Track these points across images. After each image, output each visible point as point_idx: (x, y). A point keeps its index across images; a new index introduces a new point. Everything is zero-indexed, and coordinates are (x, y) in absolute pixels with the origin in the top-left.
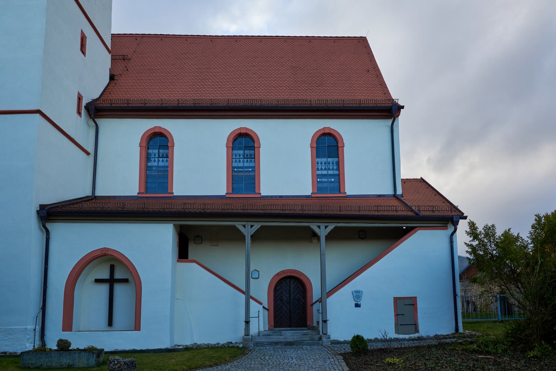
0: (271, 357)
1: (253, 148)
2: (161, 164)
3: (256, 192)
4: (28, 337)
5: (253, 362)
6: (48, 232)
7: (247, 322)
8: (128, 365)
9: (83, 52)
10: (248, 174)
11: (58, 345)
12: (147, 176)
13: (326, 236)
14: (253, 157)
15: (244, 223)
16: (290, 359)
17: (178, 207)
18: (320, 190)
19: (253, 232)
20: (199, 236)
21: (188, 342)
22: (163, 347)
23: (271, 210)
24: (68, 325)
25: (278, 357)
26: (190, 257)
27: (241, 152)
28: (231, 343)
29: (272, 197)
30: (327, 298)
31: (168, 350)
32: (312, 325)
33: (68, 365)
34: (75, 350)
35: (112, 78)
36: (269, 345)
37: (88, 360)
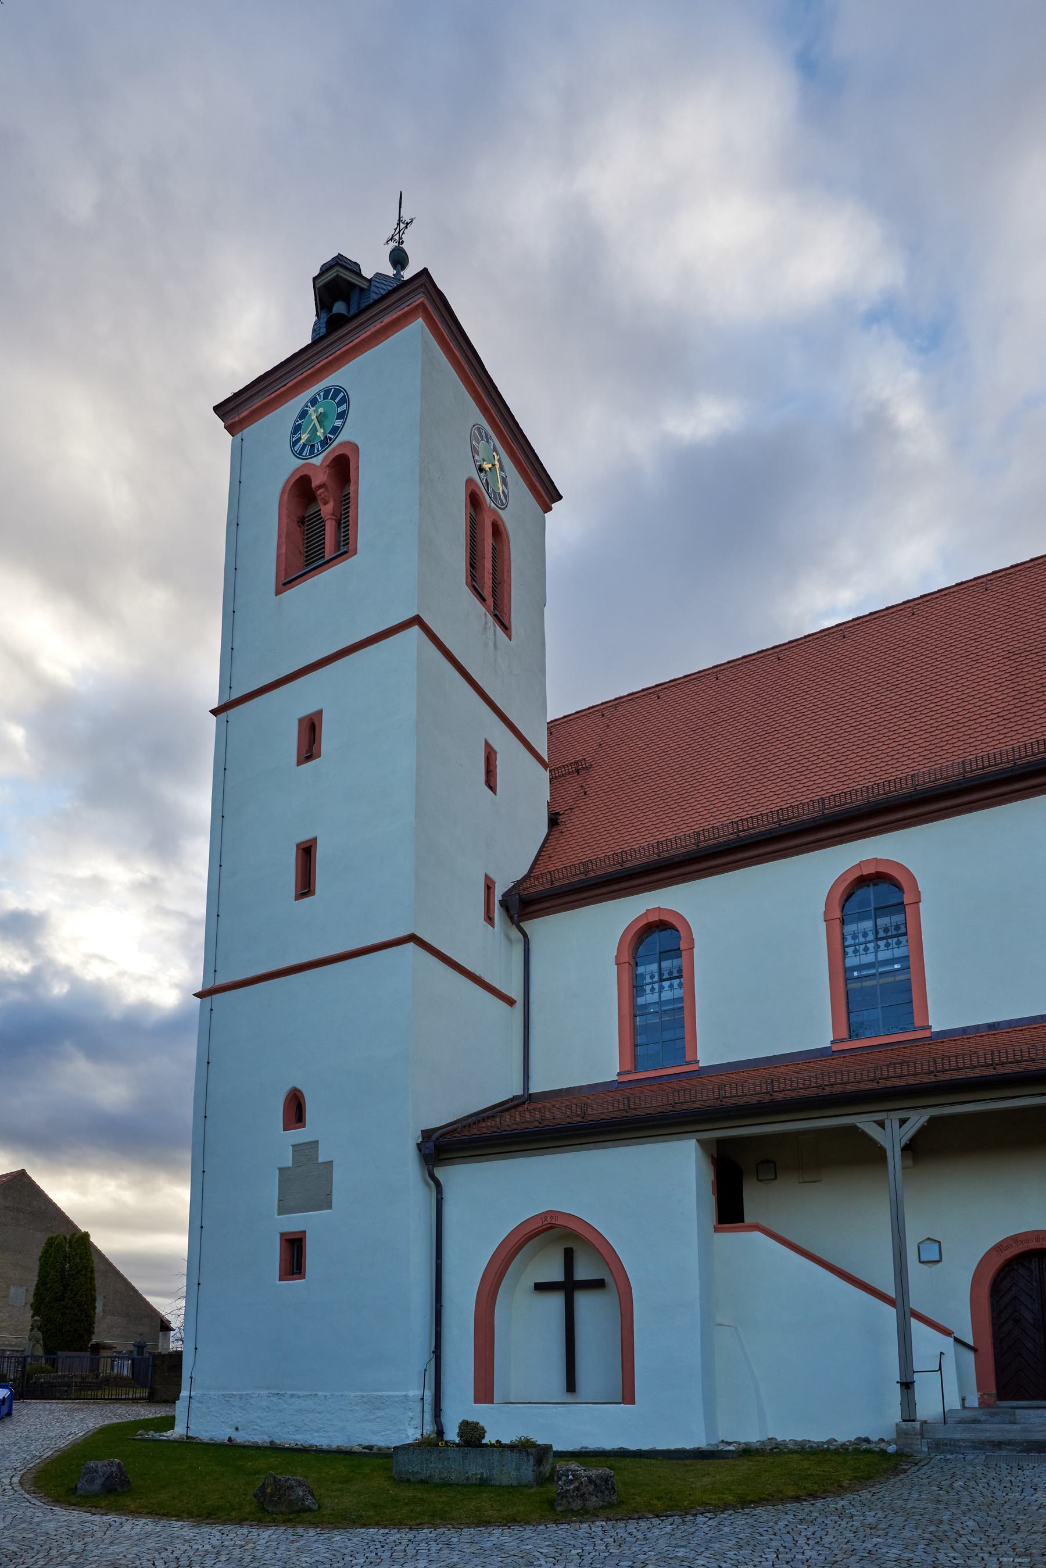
0: (972, 1484)
1: (900, 907)
2: (667, 995)
3: (918, 1022)
4: (411, 1414)
5: (915, 1495)
6: (438, 1185)
7: (907, 1386)
8: (596, 1485)
9: (491, 783)
10: (891, 979)
11: (460, 1435)
12: (635, 1030)
13: (905, 1149)
14: (902, 930)
16: (1029, 1491)
17: (705, 1097)
18: (853, 1033)
20: (767, 1162)
21: (752, 1435)
22: (689, 1446)
23: (958, 1069)
25: (993, 1483)
26: (748, 1219)
27: (868, 925)
28: (867, 1440)
29: (964, 1030)
31: (699, 1454)
33: (481, 1479)
34: (492, 1445)
35: (554, 821)
36: (975, 1448)
37: (518, 1469)
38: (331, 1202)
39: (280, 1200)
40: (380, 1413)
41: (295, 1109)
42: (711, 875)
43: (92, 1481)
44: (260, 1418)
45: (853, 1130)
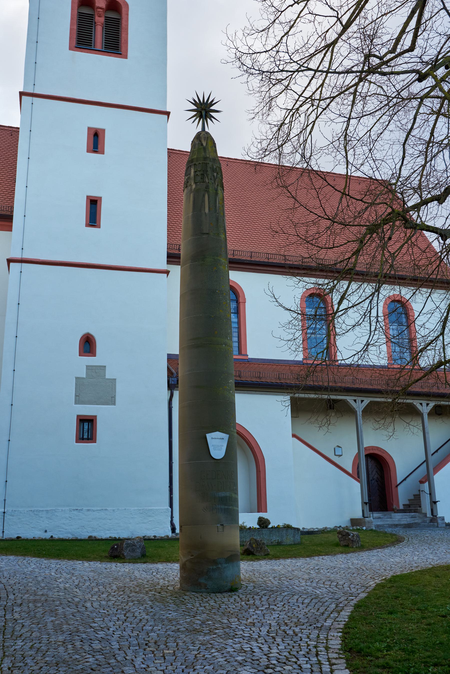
15: (355, 398)
19: (363, 408)
24: (261, 504)
30: (435, 473)
32: (398, 509)
36: (390, 527)
37: (294, 537)
39: (76, 396)
41: (88, 345)
42: (253, 272)
43: (133, 551)
44: (64, 524)
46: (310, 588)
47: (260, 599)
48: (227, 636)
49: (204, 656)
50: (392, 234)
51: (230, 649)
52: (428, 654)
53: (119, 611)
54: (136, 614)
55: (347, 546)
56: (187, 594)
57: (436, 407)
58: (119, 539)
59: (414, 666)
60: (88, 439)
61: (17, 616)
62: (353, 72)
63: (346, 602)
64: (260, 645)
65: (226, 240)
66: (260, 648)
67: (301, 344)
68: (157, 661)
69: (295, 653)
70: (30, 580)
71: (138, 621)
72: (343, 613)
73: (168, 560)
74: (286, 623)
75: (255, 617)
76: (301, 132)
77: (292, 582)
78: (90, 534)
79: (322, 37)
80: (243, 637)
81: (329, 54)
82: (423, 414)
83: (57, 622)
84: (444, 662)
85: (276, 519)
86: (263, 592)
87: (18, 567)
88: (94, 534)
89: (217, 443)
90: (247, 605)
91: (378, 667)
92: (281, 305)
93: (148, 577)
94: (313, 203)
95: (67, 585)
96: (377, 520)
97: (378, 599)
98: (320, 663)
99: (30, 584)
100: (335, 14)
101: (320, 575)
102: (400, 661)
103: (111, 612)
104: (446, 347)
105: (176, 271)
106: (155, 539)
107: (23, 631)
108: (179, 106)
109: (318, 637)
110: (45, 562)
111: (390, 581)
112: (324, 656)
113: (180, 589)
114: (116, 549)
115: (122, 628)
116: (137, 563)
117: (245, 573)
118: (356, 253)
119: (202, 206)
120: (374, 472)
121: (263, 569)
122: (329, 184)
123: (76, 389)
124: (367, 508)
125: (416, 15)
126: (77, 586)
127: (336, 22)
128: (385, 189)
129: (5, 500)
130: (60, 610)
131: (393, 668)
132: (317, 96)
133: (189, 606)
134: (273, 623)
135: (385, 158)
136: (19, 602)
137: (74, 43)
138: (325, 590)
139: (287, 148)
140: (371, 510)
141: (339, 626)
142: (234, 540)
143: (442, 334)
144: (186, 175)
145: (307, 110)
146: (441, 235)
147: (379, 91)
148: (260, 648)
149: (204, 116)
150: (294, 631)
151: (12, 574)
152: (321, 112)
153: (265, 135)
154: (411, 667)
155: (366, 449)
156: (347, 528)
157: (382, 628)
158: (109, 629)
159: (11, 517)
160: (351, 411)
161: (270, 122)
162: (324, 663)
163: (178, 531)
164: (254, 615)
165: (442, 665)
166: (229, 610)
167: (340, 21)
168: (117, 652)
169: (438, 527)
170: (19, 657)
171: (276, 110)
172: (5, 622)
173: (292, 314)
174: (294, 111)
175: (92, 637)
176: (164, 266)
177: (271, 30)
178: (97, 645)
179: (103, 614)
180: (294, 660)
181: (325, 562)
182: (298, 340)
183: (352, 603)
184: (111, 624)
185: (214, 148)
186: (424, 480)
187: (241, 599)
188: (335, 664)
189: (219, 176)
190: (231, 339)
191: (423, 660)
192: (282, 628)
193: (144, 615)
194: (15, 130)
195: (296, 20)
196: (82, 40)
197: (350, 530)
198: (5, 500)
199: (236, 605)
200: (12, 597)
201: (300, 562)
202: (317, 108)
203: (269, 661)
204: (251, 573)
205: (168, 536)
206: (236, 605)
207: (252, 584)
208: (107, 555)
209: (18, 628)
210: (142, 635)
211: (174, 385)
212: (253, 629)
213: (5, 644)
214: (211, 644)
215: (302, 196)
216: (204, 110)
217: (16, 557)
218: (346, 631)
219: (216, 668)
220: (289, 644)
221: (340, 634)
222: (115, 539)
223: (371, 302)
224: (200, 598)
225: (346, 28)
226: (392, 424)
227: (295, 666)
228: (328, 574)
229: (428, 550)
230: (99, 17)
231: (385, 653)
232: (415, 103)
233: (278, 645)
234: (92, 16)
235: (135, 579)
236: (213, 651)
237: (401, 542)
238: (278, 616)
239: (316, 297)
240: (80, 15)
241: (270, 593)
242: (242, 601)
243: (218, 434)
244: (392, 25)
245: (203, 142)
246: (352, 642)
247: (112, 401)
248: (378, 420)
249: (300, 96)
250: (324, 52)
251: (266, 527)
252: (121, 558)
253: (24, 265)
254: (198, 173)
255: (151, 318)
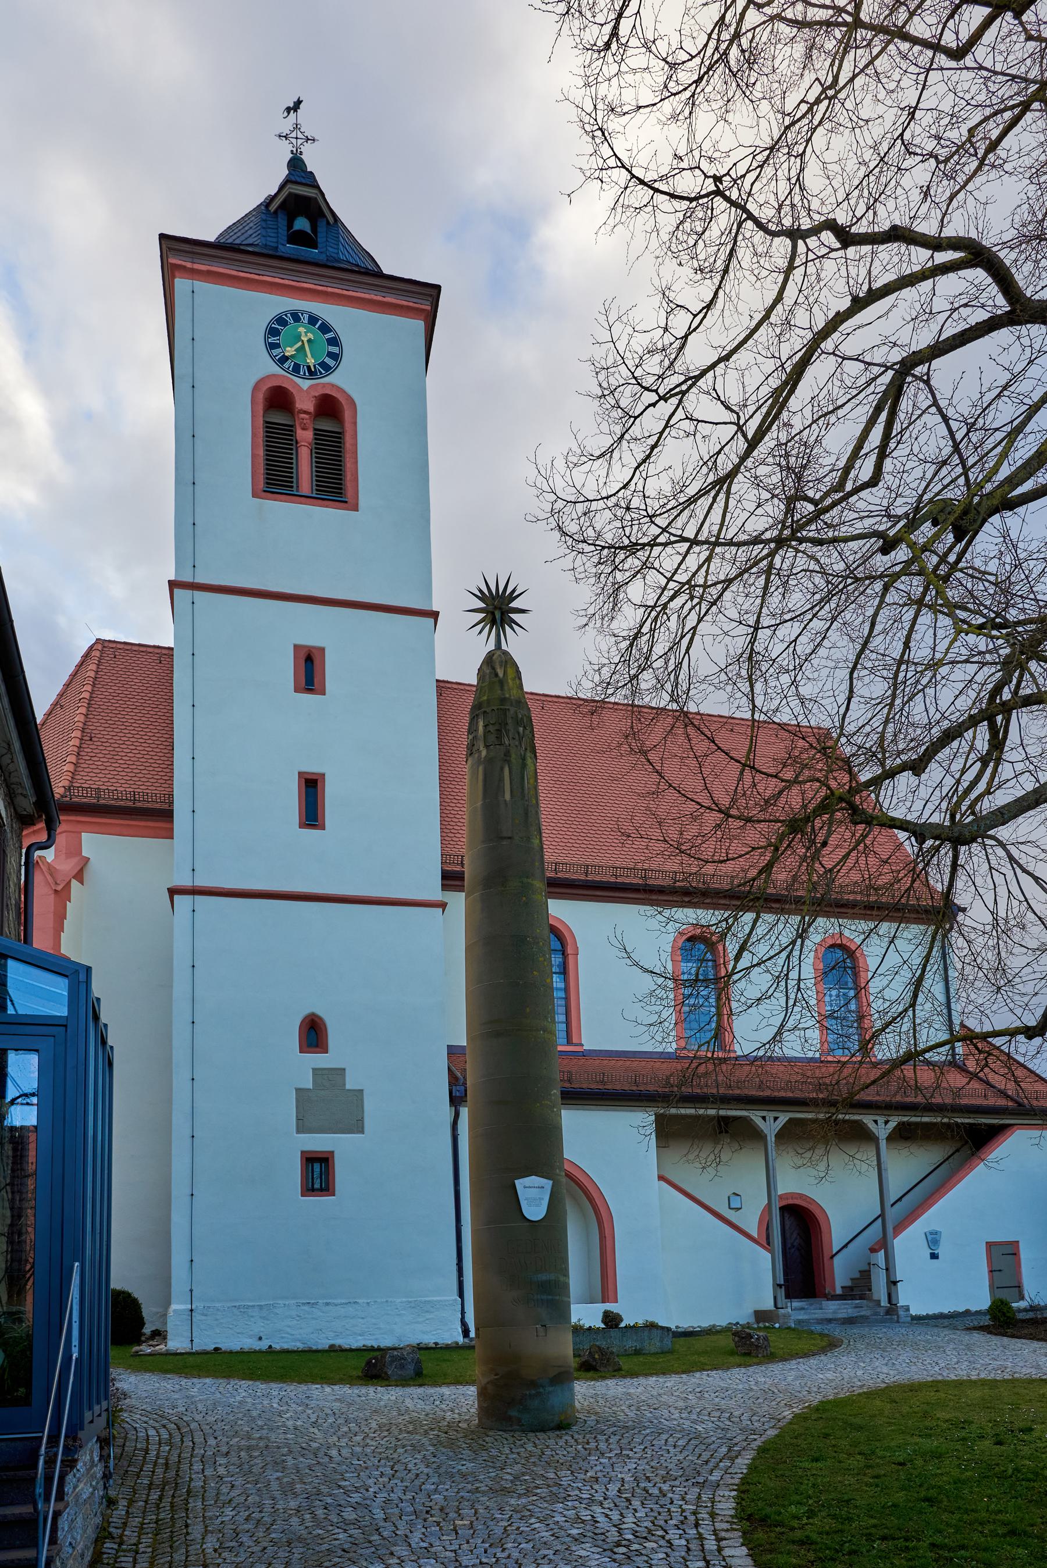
15: (764, 1113)
37: (661, 1341)
38: (363, 1127)
39: (298, 1119)
40: (428, 1316)
41: (314, 1033)
43: (402, 1367)
44: (289, 1326)
45: (746, 1121)
46: (688, 1423)
47: (607, 1440)
48: (554, 1498)
49: (518, 1528)
50: (829, 833)
51: (558, 1518)
52: (874, 1521)
53: (383, 1461)
54: (410, 1466)
55: (748, 1354)
56: (490, 1433)
57: (901, 1126)
58: (379, 1349)
59: (850, 1541)
60: (321, 1190)
61: (222, 1471)
62: (762, 542)
63: (745, 1444)
64: (606, 1511)
65: (542, 848)
66: (607, 1516)
67: (671, 1030)
68: (444, 1538)
69: (662, 1523)
70: (240, 1415)
71: (413, 1477)
72: (739, 1461)
73: (457, 1382)
74: (648, 1478)
75: (598, 1468)
76: (671, 648)
77: (658, 1413)
78: (332, 1342)
79: (710, 464)
80: (580, 1500)
81: (722, 496)
82: (878, 1139)
83: (285, 1480)
84: (898, 1534)
85: (632, 1312)
86: (611, 1430)
87: (219, 1395)
88: (338, 1342)
89: (533, 1196)
90: (586, 1449)
91: (793, 1542)
92: (636, 964)
93: (428, 1408)
94: (692, 784)
95: (299, 1423)
96: (796, 1311)
97: (796, 1438)
98: (701, 1537)
99: (240, 1422)
100: (733, 418)
101: (703, 1402)
102: (828, 1533)
103: (369, 1463)
104: (918, 1028)
105: (458, 901)
106: (436, 1348)
107: (232, 1494)
108: (454, 597)
109: (699, 1497)
110: (263, 1386)
111: (817, 1409)
112: (708, 1528)
113: (478, 1426)
114: (375, 1365)
115: (388, 1487)
116: (409, 1385)
117: (582, 1400)
118: (768, 868)
119: (500, 788)
120: (795, 1235)
121: (611, 1393)
122: (719, 748)
123: (297, 1107)
124: (782, 1293)
125: (883, 416)
126: (314, 1424)
127: (736, 433)
128: (823, 743)
129: (191, 1291)
130: (290, 1461)
131: (816, 1543)
132: (700, 580)
133: (494, 1452)
134: (628, 1478)
135: (820, 695)
136: (224, 1449)
137: (261, 485)
138: (710, 1424)
139: (647, 680)
140: (788, 1296)
141: (733, 1481)
142: (564, 1348)
143: (913, 1005)
144: (469, 732)
145: (682, 607)
146: (914, 834)
147: (813, 566)
148: (607, 1516)
149: (499, 621)
150: (660, 1488)
151: (210, 1407)
152: (708, 610)
153: (606, 656)
154: (846, 1542)
155: (781, 1197)
156: (748, 1326)
157: (801, 1484)
158: (367, 1490)
159: (203, 1318)
160: (755, 1135)
161: (616, 632)
162: (708, 1537)
163: (472, 1334)
164: (597, 1465)
165: (894, 1539)
166: (557, 1457)
167: (743, 432)
168: (382, 1524)
169: (898, 1322)
170: (228, 1531)
171: (627, 609)
172: (204, 1481)
173: (655, 979)
174: (658, 609)
175: (342, 1502)
176: (435, 893)
177: (616, 454)
178: (349, 1514)
179: (358, 1467)
180: (661, 1533)
181: (712, 1380)
182: (666, 1024)
183: (754, 1445)
184: (371, 1482)
185: (518, 681)
186: (877, 1247)
187: (576, 1441)
188: (725, 1539)
189: (527, 732)
190: (553, 1021)
191: (865, 1531)
192: (642, 1485)
193: (422, 1467)
194: (166, 652)
195: (661, 433)
196: (276, 478)
197: (755, 1329)
198: (191, 1291)
199: (569, 1449)
200: (212, 1442)
201: (671, 1381)
202: (699, 603)
203: (621, 1535)
204: (591, 1400)
205: (457, 1343)
206: (569, 1449)
207: (593, 1417)
208: (360, 1374)
209: (224, 1489)
210: (421, 1498)
211: (461, 1097)
212: (595, 1487)
213: (206, 1514)
214: (529, 1510)
215: (672, 772)
216: (498, 609)
217: (215, 1381)
218: (743, 1488)
219: (538, 1546)
220: (652, 1510)
221: (734, 1493)
222: (372, 1349)
223: (788, 957)
224: (511, 1440)
225: (753, 444)
226: (825, 1158)
227: (662, 1542)
228: (717, 1400)
229: (881, 1359)
230: (303, 429)
231: (805, 1521)
232: (878, 586)
233: (635, 1510)
234: (290, 429)
235: (406, 1411)
236: (533, 1520)
237: (836, 1346)
238: (634, 1466)
239: (698, 943)
240: (269, 426)
241: (624, 1431)
242: (578, 1444)
243: (533, 1180)
244: (838, 441)
245: (499, 668)
246: (753, 1504)
247: (358, 1127)
248: (800, 1151)
249: (669, 580)
250: (713, 493)
251: (617, 1326)
252: (383, 1379)
253: (199, 898)
254: (491, 728)
255: (421, 979)
